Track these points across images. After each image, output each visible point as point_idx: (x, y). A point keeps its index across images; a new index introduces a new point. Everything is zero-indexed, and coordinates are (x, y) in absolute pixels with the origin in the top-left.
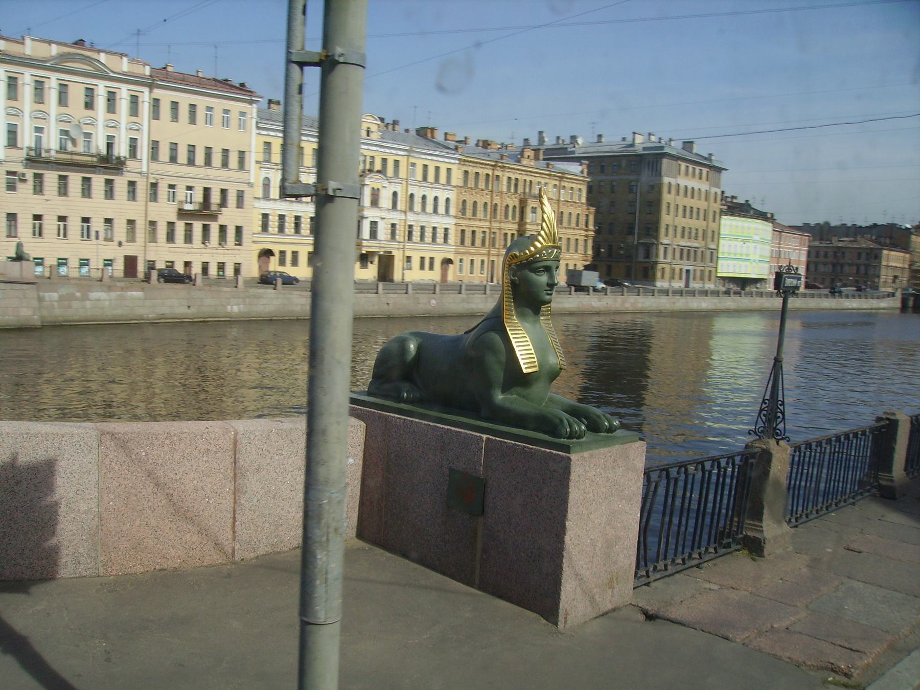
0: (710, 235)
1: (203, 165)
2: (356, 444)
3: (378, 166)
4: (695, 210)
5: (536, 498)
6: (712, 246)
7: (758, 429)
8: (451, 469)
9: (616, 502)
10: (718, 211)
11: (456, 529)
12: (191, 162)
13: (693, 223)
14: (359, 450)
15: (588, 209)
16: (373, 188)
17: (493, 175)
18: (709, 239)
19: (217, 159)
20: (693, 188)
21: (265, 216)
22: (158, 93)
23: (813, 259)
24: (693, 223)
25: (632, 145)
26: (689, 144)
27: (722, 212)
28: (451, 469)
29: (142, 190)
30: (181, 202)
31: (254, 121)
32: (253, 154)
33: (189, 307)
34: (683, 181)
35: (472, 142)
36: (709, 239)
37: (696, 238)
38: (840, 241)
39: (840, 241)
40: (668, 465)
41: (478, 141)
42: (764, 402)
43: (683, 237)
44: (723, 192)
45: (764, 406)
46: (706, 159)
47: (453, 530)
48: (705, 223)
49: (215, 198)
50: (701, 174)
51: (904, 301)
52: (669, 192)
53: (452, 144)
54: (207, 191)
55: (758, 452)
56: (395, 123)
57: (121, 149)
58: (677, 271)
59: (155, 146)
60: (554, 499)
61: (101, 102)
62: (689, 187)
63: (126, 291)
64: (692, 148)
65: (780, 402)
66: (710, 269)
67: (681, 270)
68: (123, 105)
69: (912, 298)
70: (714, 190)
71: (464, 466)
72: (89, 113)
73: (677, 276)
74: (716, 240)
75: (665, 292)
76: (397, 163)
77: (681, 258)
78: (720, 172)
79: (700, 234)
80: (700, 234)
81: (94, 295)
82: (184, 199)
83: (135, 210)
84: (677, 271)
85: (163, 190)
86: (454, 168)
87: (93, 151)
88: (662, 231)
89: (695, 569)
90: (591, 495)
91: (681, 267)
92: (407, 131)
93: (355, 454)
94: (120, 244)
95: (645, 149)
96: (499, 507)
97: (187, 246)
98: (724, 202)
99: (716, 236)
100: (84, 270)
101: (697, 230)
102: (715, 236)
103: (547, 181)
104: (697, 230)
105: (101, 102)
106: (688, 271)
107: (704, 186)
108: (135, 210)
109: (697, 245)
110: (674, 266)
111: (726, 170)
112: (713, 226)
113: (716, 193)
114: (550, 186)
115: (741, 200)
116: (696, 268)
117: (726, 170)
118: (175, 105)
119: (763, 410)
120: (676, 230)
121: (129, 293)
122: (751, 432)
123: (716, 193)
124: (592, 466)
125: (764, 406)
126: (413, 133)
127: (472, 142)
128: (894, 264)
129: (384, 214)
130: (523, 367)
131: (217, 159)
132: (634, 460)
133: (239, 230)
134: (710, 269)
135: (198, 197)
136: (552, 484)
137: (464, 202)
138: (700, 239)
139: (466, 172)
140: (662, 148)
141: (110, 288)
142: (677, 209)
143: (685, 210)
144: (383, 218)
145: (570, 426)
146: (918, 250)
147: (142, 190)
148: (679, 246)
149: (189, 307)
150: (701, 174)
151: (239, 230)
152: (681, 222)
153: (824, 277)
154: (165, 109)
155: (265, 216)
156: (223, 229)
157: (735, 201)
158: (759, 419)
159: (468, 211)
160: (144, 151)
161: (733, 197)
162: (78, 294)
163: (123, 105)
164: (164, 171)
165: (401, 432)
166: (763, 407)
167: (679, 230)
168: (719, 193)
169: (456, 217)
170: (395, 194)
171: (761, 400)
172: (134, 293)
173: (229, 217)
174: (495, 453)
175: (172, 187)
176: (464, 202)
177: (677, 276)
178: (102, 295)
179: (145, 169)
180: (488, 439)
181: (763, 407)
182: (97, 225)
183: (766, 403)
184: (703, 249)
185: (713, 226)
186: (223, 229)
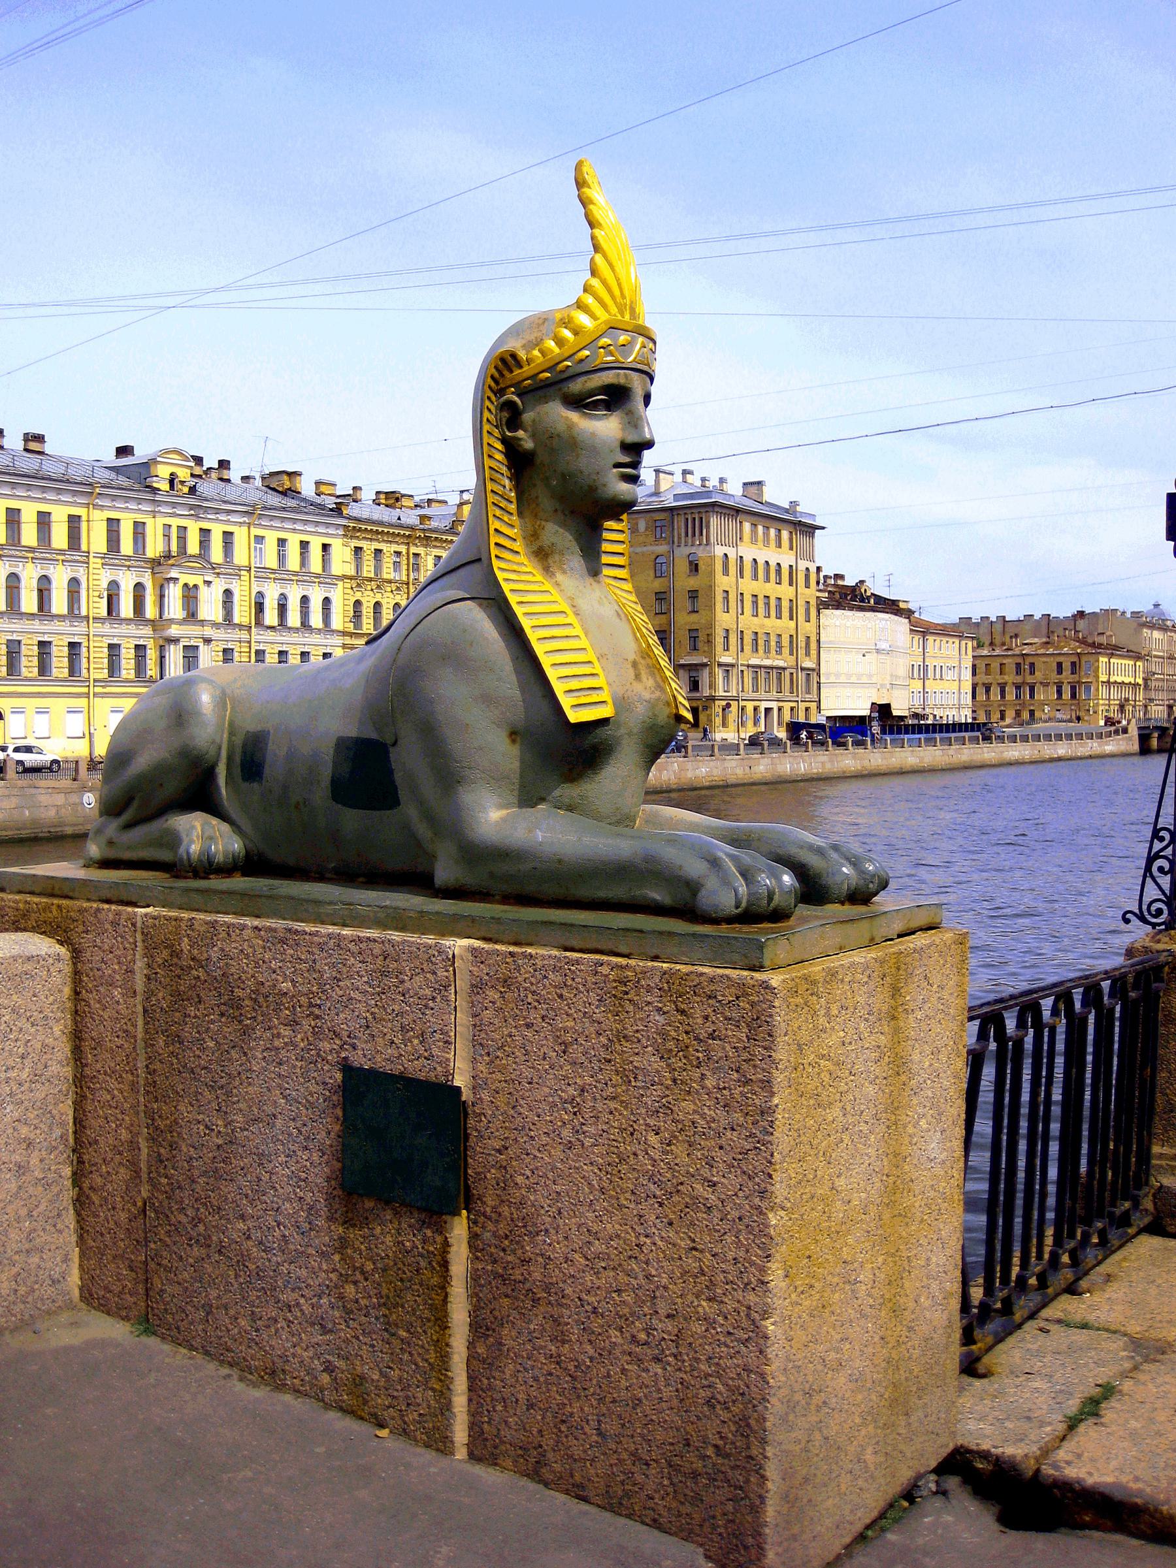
0: (802, 644)
2: (47, 1012)
4: (773, 602)
5: (653, 1139)
6: (808, 664)
7: (1149, 909)
8: (347, 1068)
10: (813, 602)
13: (772, 625)
14: (58, 1033)
15: (343, 1244)
16: (186, 585)
17: (408, 553)
18: (802, 652)
20: (767, 562)
23: (982, 678)
24: (772, 625)
25: (657, 493)
26: (755, 487)
27: (822, 605)
28: (347, 1068)
34: (748, 552)
35: (367, 495)
36: (802, 652)
37: (779, 652)
38: (1026, 644)
39: (1026, 644)
40: (1001, 1001)
41: (378, 493)
42: (1156, 835)
43: (756, 649)
44: (819, 569)
45: (1157, 846)
46: (787, 511)
48: (793, 624)
51: (1144, 738)
52: (726, 572)
53: (330, 502)
55: (1167, 963)
56: (224, 464)
62: (773, 564)
64: (761, 494)
66: (808, 705)
67: (756, 709)
69: (1156, 735)
70: (803, 565)
74: (814, 652)
75: (730, 748)
78: (812, 535)
79: (785, 641)
80: (785, 641)
86: (337, 544)
88: (719, 640)
89: (1065, 1297)
90: (836, 1111)
91: (757, 703)
92: (245, 479)
93: (44, 1045)
95: (677, 497)
98: (821, 587)
99: (813, 645)
101: (779, 636)
102: (814, 645)
104: (779, 636)
106: (768, 710)
107: (786, 559)
109: (781, 664)
110: (744, 703)
111: (823, 528)
112: (808, 628)
113: (807, 569)
115: (850, 581)
116: (781, 704)
117: (823, 528)
119: (1157, 856)
120: (742, 639)
122: (1129, 916)
123: (807, 569)
124: (835, 1012)
125: (1157, 846)
126: (258, 482)
127: (367, 495)
128: (1119, 679)
129: (208, 632)
130: (566, 702)
132: (941, 987)
134: (808, 705)
136: (710, 1083)
137: (358, 603)
138: (786, 651)
139: (358, 550)
140: (708, 494)
142: (742, 601)
143: (755, 603)
144: (207, 641)
145: (746, 874)
146: (1154, 653)
148: (748, 666)
152: (750, 623)
153: (1002, 708)
157: (840, 582)
159: (365, 620)
161: (838, 577)
166: (1154, 850)
167: (748, 639)
168: (813, 570)
169: (344, 633)
171: (1148, 832)
176: (358, 603)
180: (474, 951)
181: (1154, 850)
183: (1162, 839)
184: (792, 671)
185: (808, 628)
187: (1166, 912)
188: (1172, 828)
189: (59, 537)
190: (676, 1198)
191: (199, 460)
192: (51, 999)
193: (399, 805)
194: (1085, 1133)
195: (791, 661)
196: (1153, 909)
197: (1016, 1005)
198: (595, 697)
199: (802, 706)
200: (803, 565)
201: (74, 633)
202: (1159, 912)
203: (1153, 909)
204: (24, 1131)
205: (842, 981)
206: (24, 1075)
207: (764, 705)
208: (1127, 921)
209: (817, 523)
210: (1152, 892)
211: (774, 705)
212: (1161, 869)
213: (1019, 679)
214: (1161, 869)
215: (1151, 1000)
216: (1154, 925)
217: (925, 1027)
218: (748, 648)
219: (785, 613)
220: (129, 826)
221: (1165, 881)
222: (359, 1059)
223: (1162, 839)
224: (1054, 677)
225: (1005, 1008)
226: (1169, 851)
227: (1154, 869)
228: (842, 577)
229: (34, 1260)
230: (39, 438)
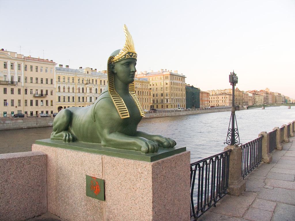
1: (40, 83)
3: (91, 82)
8: (87, 176)
9: (179, 185)
11: (92, 208)
12: (37, 83)
19: (44, 81)
21: (59, 97)
22: (26, 63)
28: (87, 176)
29: (22, 91)
30: (34, 94)
31: (55, 70)
32: (55, 79)
33: (37, 124)
42: (229, 130)
45: (229, 131)
47: (91, 208)
49: (44, 93)
50: (180, 79)
54: (42, 91)
57: (16, 80)
58: (176, 105)
59: (26, 79)
60: (144, 190)
61: (9, 66)
62: (177, 83)
63: (17, 120)
65: (236, 129)
68: (16, 67)
70: (183, 83)
71: (93, 173)
72: (6, 69)
73: (176, 107)
76: (96, 80)
77: (176, 102)
81: (7, 122)
82: (35, 93)
83: (20, 97)
84: (176, 105)
85: (29, 92)
87: (7, 80)
90: (165, 184)
94: (16, 107)
96: (113, 195)
97: (37, 106)
100: (5, 115)
103: (138, 83)
105: (9, 66)
108: (20, 97)
109: (180, 98)
114: (139, 85)
118: (31, 67)
119: (229, 133)
121: (18, 121)
124: (164, 168)
125: (229, 131)
129: (93, 95)
131: (44, 81)
132: (185, 161)
133: (52, 102)
135: (39, 93)
141: (12, 120)
147: (22, 91)
149: (37, 124)
150: (180, 79)
151: (52, 102)
154: (29, 68)
155: (59, 97)
156: (47, 101)
158: (228, 138)
160: (22, 80)
162: (2, 122)
163: (16, 67)
164: (29, 86)
165: (62, 157)
170: (96, 89)
172: (20, 121)
173: (49, 98)
174: (108, 165)
175: (31, 90)
177: (176, 107)
178: (9, 122)
179: (23, 85)
182: (9, 102)
183: (230, 130)
186: (47, 101)
187: (230, 143)
188: (231, 129)
189: (71, 80)
190: (137, 200)
191: (92, 69)
192: (43, 162)
193: (46, 156)
194: (200, 192)
195: (182, 97)
196: (229, 142)
197: (195, 165)
198: (126, 114)
199: (184, 104)
200: (183, 83)
201: (73, 95)
202: (230, 142)
203: (229, 142)
204: (38, 184)
205: (165, 162)
206: (38, 175)
207: (178, 104)
208: (225, 144)
209: (185, 76)
210: (228, 139)
211: (179, 104)
212: (230, 135)
213: (217, 100)
214: (230, 135)
215: (228, 156)
216: (229, 144)
217: (182, 168)
218: (175, 96)
219: (181, 90)
220: (56, 133)
221: (230, 137)
222: (88, 174)
223: (230, 130)
224: (222, 99)
225: (200, 163)
226: (231, 133)
227: (229, 136)
228: (189, 85)
229: (40, 204)
230: (68, 66)
